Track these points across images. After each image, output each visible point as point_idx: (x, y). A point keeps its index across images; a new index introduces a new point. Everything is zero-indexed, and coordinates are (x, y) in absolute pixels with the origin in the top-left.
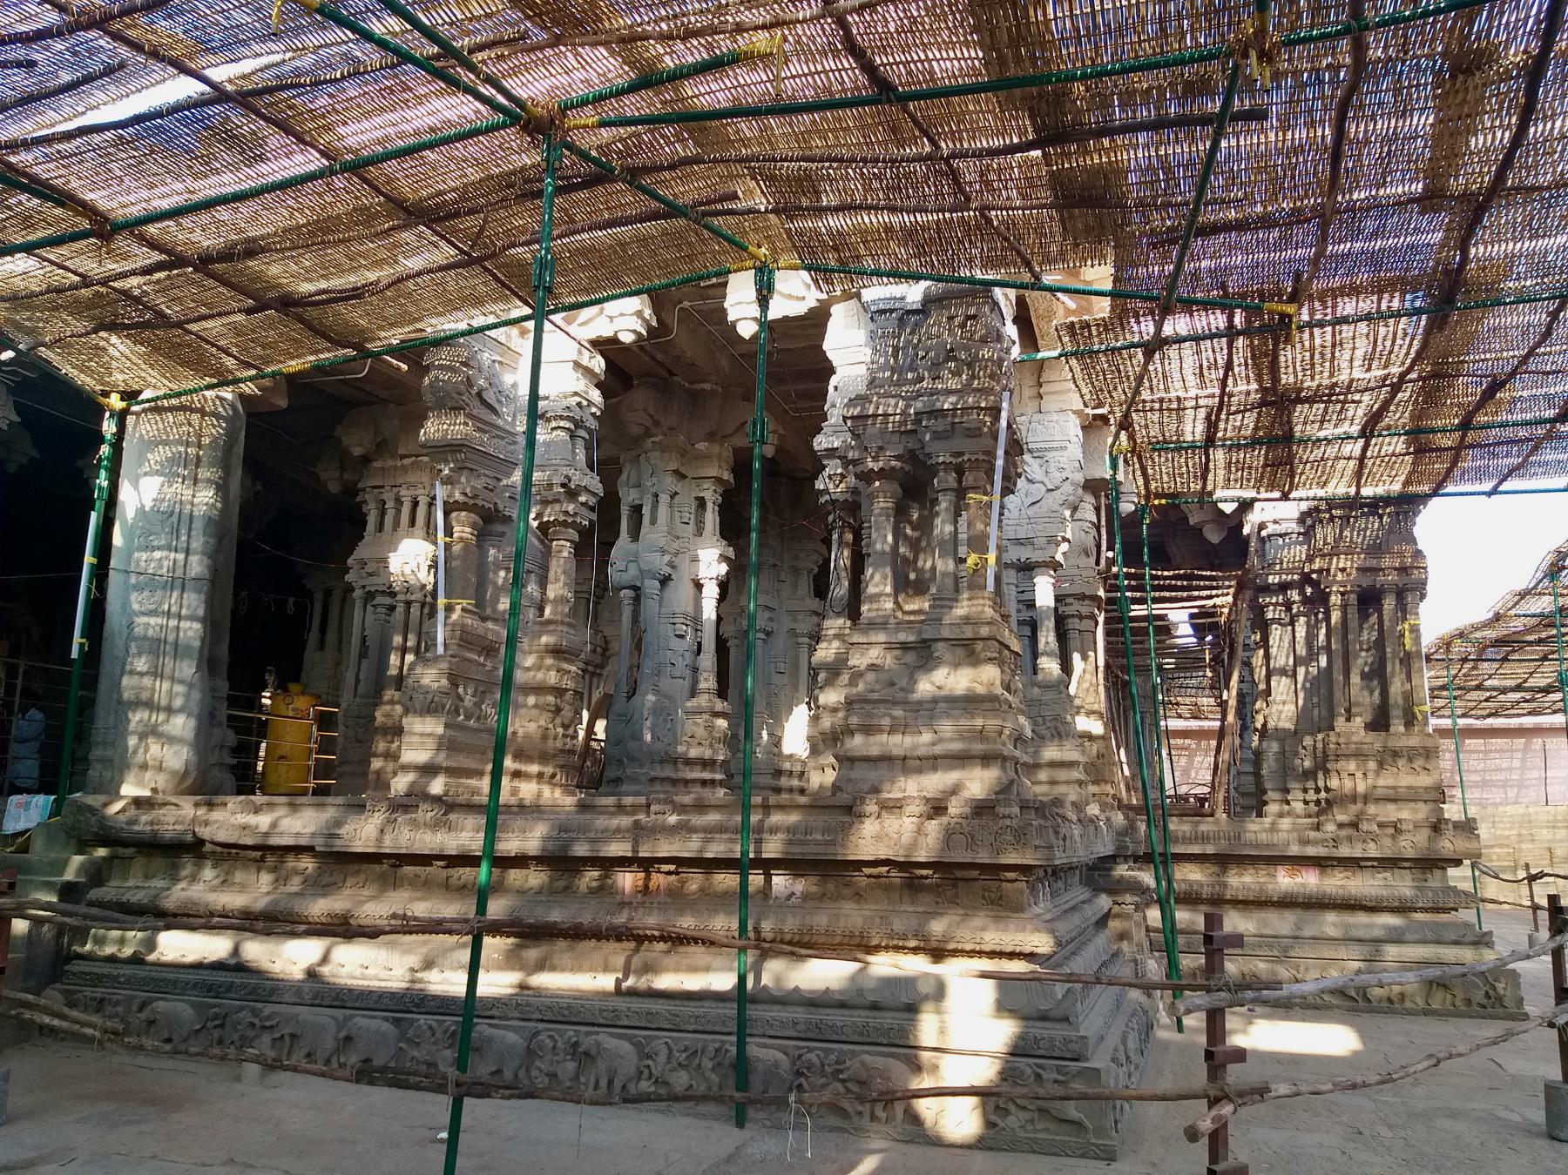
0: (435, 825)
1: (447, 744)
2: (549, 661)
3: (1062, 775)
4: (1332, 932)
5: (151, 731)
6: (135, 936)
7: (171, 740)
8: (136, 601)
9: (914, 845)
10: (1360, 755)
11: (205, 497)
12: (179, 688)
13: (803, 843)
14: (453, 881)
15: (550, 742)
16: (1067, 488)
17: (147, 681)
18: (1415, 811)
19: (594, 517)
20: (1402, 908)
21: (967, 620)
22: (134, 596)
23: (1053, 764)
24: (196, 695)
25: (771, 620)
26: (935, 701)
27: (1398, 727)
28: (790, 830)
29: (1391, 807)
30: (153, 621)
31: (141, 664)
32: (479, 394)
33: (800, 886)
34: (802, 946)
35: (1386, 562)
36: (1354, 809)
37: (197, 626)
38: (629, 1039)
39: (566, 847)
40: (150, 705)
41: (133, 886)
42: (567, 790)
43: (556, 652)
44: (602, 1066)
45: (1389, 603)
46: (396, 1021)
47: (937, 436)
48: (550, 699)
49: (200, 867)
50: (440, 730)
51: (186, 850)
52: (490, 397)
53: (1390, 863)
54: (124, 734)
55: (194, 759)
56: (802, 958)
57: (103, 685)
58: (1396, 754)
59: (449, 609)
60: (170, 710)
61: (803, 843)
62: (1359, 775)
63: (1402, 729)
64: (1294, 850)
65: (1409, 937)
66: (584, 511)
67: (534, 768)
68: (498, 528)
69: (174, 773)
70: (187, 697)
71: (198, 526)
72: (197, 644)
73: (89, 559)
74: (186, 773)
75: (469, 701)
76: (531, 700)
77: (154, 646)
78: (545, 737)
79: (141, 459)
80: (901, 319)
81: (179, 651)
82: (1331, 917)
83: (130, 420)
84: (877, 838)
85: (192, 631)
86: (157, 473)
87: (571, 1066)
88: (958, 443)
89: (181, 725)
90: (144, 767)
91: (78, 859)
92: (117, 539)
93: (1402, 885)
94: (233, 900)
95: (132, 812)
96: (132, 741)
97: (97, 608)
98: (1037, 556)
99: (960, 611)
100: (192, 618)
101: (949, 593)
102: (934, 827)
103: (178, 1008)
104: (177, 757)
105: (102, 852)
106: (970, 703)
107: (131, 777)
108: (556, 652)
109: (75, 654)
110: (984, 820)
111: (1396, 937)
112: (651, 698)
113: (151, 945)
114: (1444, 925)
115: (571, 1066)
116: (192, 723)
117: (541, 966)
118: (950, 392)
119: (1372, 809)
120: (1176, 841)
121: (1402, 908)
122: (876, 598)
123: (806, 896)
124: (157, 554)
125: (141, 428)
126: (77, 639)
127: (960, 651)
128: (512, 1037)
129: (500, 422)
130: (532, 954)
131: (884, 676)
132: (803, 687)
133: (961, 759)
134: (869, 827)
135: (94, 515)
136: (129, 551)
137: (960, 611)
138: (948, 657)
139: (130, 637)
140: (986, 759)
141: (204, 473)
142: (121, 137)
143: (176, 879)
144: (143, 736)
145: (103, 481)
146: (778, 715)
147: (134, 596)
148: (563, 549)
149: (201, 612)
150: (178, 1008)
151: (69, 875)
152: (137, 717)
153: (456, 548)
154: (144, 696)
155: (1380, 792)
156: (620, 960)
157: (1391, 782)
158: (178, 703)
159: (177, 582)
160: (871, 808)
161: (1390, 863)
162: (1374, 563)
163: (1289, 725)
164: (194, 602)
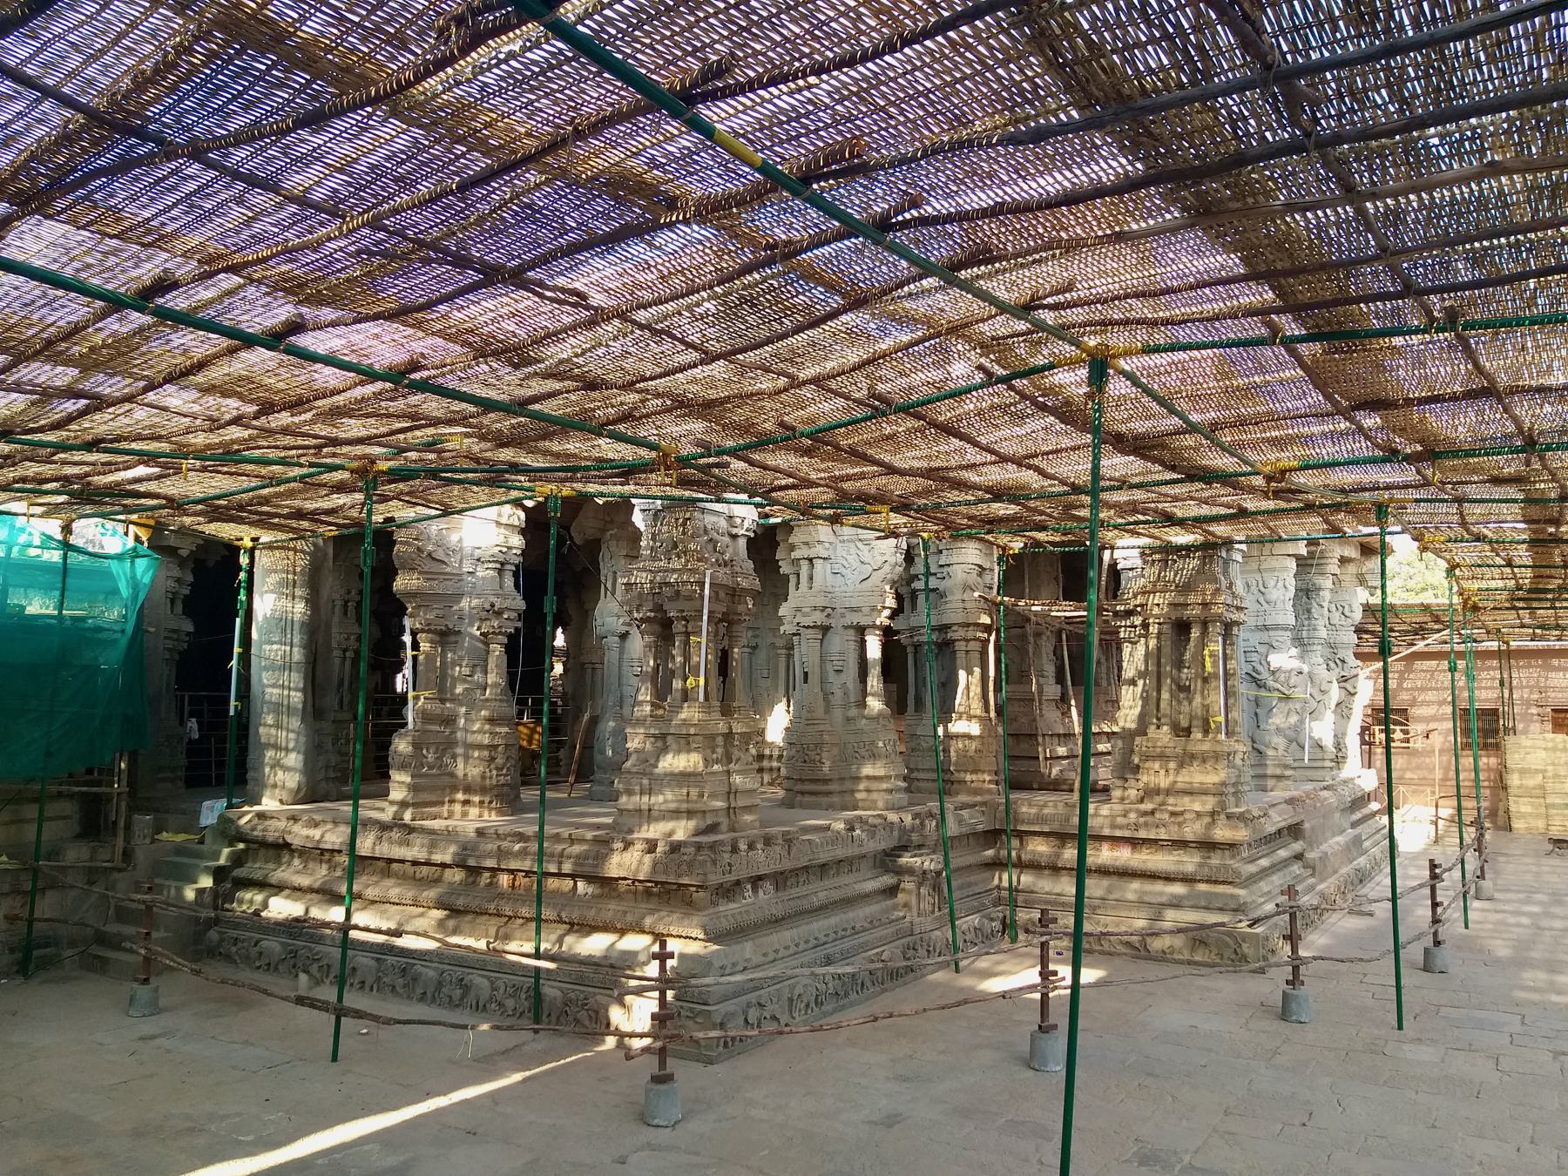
0: (400, 843)
1: (413, 788)
2: (487, 727)
3: (874, 785)
4: (1131, 896)
5: (277, 764)
6: (259, 898)
7: (286, 769)
8: (266, 677)
9: (637, 870)
10: (1163, 757)
11: (300, 607)
12: (292, 736)
13: (582, 865)
14: (418, 876)
15: (488, 782)
16: (887, 568)
17: (273, 731)
18: (1204, 803)
19: (520, 624)
20: (1187, 880)
21: (685, 722)
22: (264, 674)
23: (868, 778)
24: (303, 739)
25: (756, 636)
26: (666, 775)
27: (1197, 735)
28: (578, 857)
29: (1187, 799)
30: (275, 691)
31: (270, 720)
32: (429, 555)
33: (590, 890)
34: (586, 928)
35: (1192, 599)
36: (1158, 799)
37: (299, 694)
38: (488, 978)
39: (465, 860)
40: (277, 747)
41: (254, 869)
42: (500, 812)
43: (491, 721)
44: (472, 994)
45: (1195, 633)
46: (378, 960)
47: (670, 599)
48: (486, 753)
49: (292, 857)
50: (409, 779)
51: (281, 848)
52: (440, 555)
53: (1181, 844)
54: (262, 765)
55: (304, 780)
56: (589, 934)
57: (252, 731)
58: (1193, 757)
59: (416, 698)
60: (287, 750)
61: (582, 865)
62: (1162, 772)
63: (1199, 736)
64: (1106, 832)
65: (1187, 903)
66: (508, 623)
67: (476, 799)
68: (453, 639)
69: (291, 790)
70: (297, 741)
71: (296, 627)
72: (300, 706)
73: (237, 650)
74: (299, 789)
75: (431, 757)
76: (476, 754)
77: (277, 708)
78: (483, 777)
79: (264, 583)
80: (655, 515)
81: (290, 710)
82: (1136, 885)
83: (257, 553)
84: (620, 865)
85: (297, 698)
86: (272, 592)
87: (459, 992)
88: (682, 604)
89: (294, 759)
90: (275, 786)
91: (226, 851)
92: (255, 635)
93: (1189, 862)
94: (304, 881)
95: (256, 821)
96: (267, 770)
97: (245, 680)
98: (864, 621)
99: (683, 716)
100: (296, 690)
101: (677, 703)
102: (648, 859)
103: (272, 945)
104: (292, 780)
105: (241, 846)
106: (684, 778)
107: (268, 793)
108: (491, 721)
109: (232, 713)
110: (674, 856)
111: (1176, 904)
112: (612, 724)
113: (265, 905)
114: (1217, 895)
115: (459, 992)
116: (301, 757)
117: (455, 932)
118: (674, 571)
119: (1171, 800)
120: (1023, 822)
121: (1187, 880)
122: (641, 703)
123: (593, 896)
124: (275, 647)
125: (263, 560)
126: (233, 703)
127: (683, 741)
128: (431, 973)
129: (448, 570)
130: (451, 923)
131: (642, 756)
132: (782, 689)
133: (675, 814)
134: (615, 859)
135: (238, 620)
136: (261, 643)
137: (683, 716)
138: (674, 746)
139: (264, 702)
140: (690, 814)
141: (298, 592)
142: (315, 251)
143: (280, 864)
144: (272, 767)
145: (242, 597)
146: (761, 707)
147: (264, 674)
148: (497, 650)
149: (301, 685)
150: (272, 945)
151: (222, 861)
152: (270, 754)
153: (421, 658)
154: (272, 741)
155: (1179, 786)
156: (493, 931)
157: (1187, 779)
158: (291, 745)
159: (287, 666)
160: (618, 845)
161: (1181, 844)
162: (1182, 600)
163: (1133, 726)
164: (297, 679)
